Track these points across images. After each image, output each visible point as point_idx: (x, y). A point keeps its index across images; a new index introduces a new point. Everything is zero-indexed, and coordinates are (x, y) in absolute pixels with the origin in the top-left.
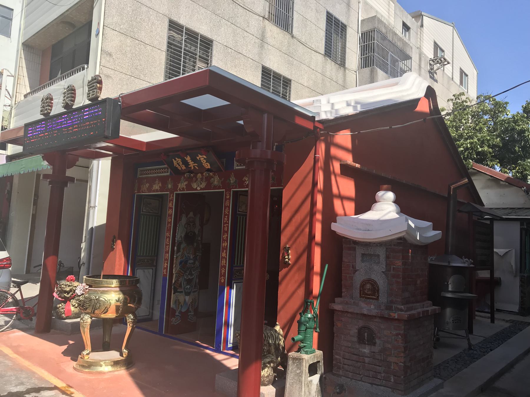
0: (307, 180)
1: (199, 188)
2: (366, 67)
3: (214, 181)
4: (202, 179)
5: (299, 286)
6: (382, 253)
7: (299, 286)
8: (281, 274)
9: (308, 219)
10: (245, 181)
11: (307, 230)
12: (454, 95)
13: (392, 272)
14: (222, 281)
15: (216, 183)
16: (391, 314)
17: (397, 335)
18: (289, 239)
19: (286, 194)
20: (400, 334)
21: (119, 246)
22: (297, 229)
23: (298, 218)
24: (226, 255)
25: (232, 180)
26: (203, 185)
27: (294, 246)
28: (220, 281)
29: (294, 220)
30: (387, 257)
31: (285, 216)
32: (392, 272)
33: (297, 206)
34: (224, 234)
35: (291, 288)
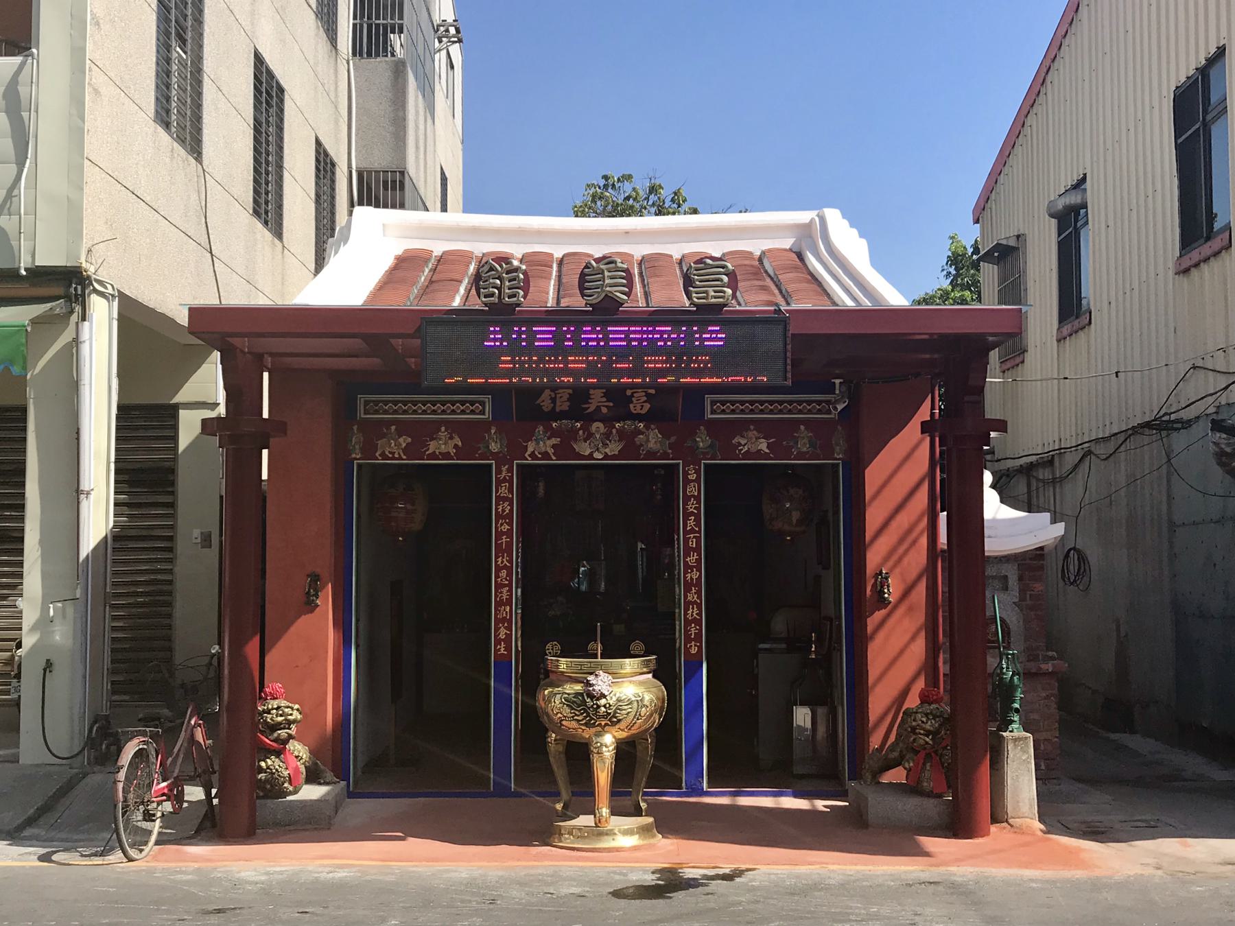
0: (917, 453)
1: (597, 455)
2: (377, 55)
3: (648, 441)
4: (607, 436)
5: (913, 638)
6: (1012, 572)
7: (913, 638)
8: (872, 622)
9: (925, 521)
10: (740, 444)
11: (924, 541)
12: (606, 178)
13: (1029, 602)
14: (694, 651)
15: (652, 445)
16: (1042, 666)
17: (1047, 697)
18: (887, 558)
19: (874, 474)
20: (1052, 695)
21: (326, 600)
22: (901, 540)
23: (903, 520)
24: (700, 597)
25: (702, 441)
26: (614, 448)
27: (897, 571)
28: (687, 650)
29: (894, 524)
30: (1021, 579)
31: (874, 517)
32: (1029, 602)
33: (899, 499)
34: (687, 554)
35: (897, 642)
